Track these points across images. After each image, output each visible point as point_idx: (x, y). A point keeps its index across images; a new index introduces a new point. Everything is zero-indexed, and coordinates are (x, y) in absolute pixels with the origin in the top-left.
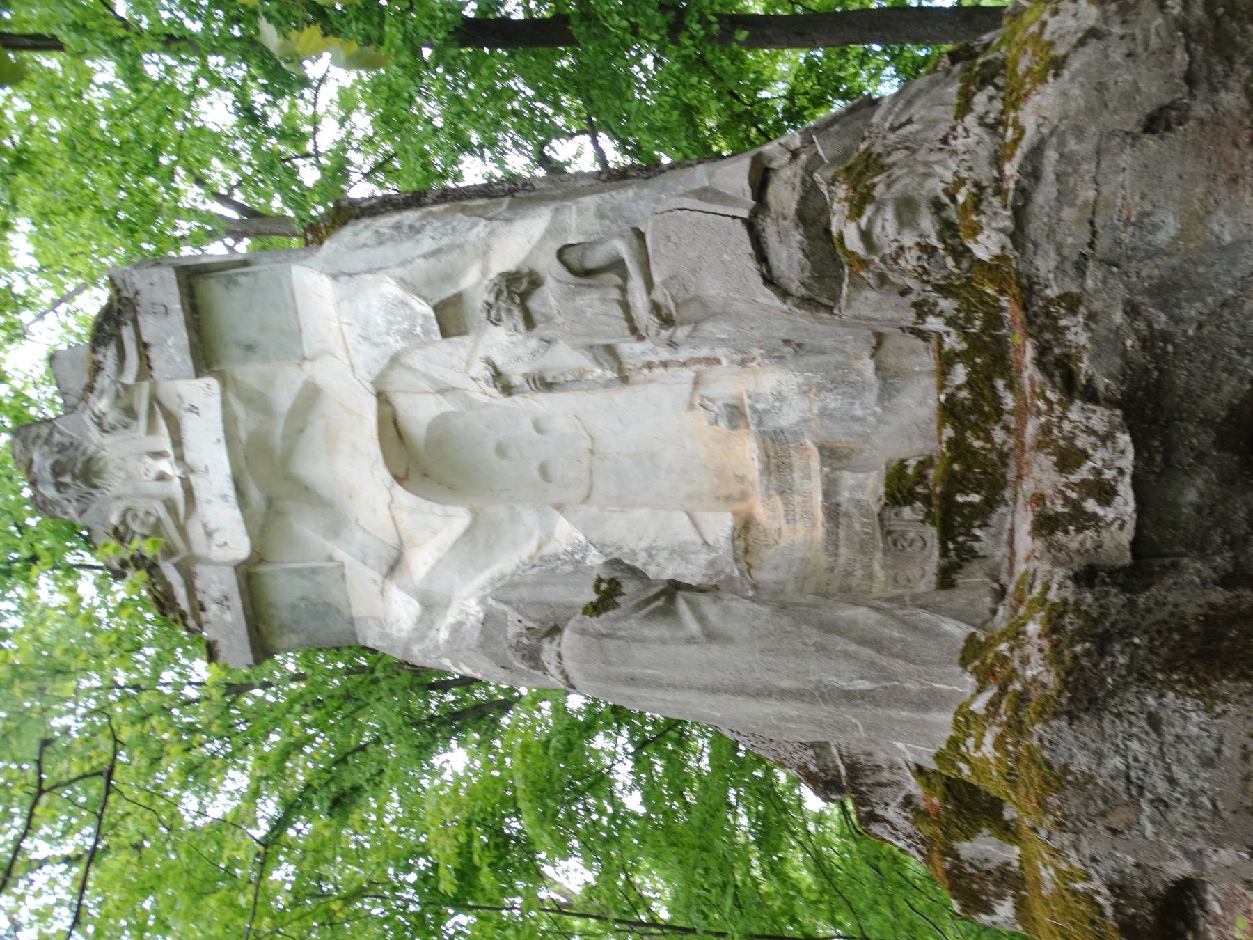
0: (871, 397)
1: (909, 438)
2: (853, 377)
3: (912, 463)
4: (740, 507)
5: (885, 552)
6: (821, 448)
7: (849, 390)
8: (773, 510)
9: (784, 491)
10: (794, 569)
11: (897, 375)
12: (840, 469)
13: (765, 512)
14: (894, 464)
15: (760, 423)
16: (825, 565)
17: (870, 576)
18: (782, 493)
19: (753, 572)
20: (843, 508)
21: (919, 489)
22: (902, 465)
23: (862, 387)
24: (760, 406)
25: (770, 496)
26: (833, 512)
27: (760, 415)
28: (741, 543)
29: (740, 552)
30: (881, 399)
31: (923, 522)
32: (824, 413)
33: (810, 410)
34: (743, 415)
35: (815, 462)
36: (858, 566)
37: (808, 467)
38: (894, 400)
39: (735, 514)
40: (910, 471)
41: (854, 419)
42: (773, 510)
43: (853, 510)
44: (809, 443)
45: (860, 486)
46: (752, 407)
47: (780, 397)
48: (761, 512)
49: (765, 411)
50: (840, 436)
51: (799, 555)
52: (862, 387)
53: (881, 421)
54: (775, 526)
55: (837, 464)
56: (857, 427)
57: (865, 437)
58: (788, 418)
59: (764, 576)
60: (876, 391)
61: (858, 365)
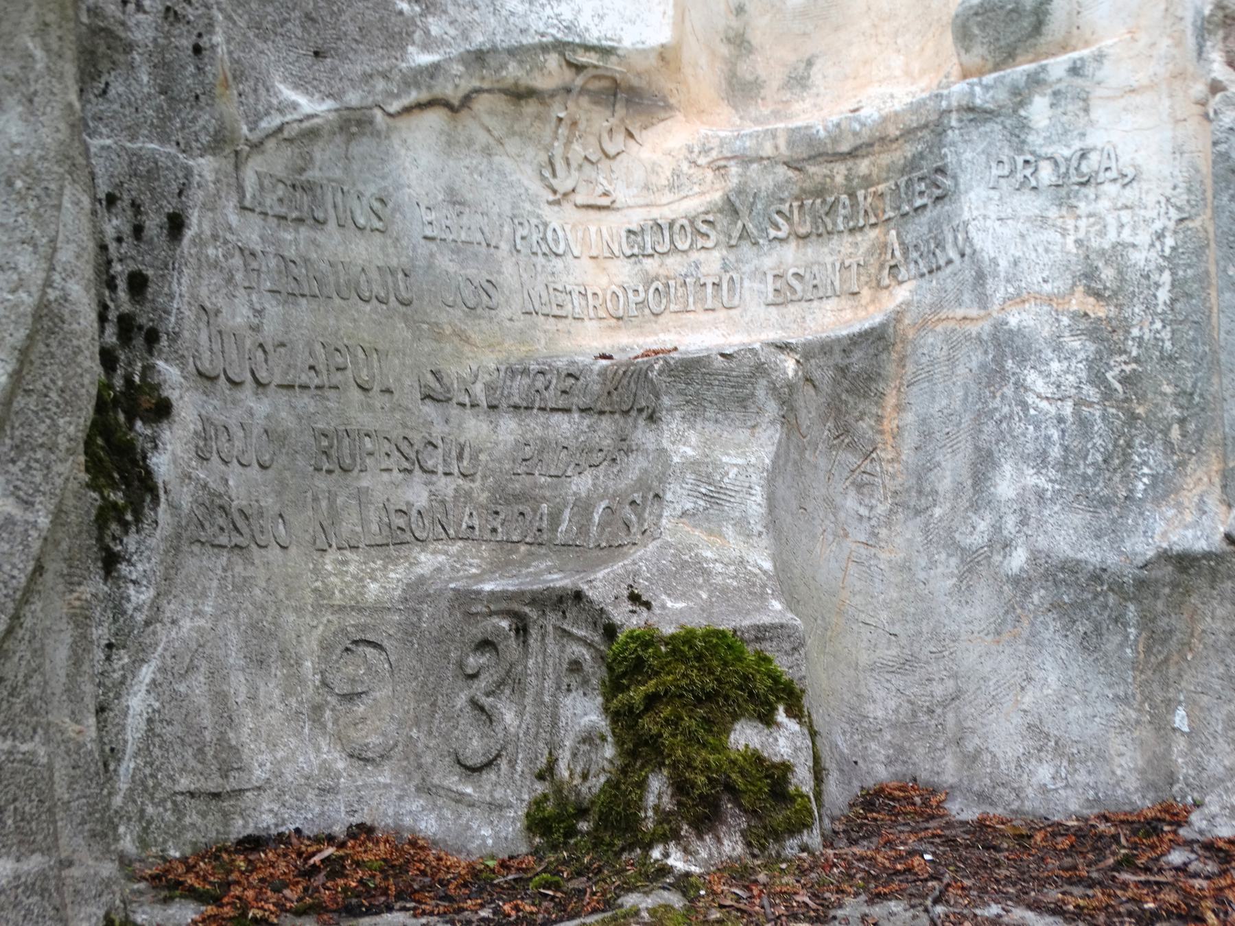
0: (1066, 535)
1: (906, 664)
2: (1149, 459)
3: (783, 741)
4: (702, 73)
5: (465, 599)
6: (876, 339)
7: (1100, 441)
8: (675, 184)
9: (737, 218)
10: (446, 263)
11: (1155, 637)
12: (789, 418)
13: (667, 164)
14: (782, 664)
15: (974, 114)
16: (452, 371)
17: (398, 537)
18: (731, 208)
19: (434, 118)
20: (643, 435)
21: (657, 789)
22: (775, 696)
23: (1110, 506)
24: (1039, 110)
25: (719, 170)
26: (632, 394)
27: (1007, 116)
28: (552, 73)
29: (513, 72)
30: (1057, 573)
31: (546, 773)
32: (1007, 348)
33: (1019, 299)
34: (1008, 56)
35: (833, 319)
36: (447, 487)
37: (818, 293)
38: (1051, 628)
39: (666, 56)
40: (745, 736)
41: (983, 465)
42: (675, 184)
43: (635, 466)
44: (902, 294)
45: (714, 499)
46: (1036, 81)
47: (1074, 182)
48: (665, 144)
49: (1019, 131)
50: (913, 410)
51: (509, 273)
52: (1110, 506)
53: (972, 563)
54: (621, 195)
55: (810, 405)
56: (951, 470)
57: (915, 497)
58: (993, 216)
59: (418, 159)
60: (1093, 555)
61: (1201, 481)
